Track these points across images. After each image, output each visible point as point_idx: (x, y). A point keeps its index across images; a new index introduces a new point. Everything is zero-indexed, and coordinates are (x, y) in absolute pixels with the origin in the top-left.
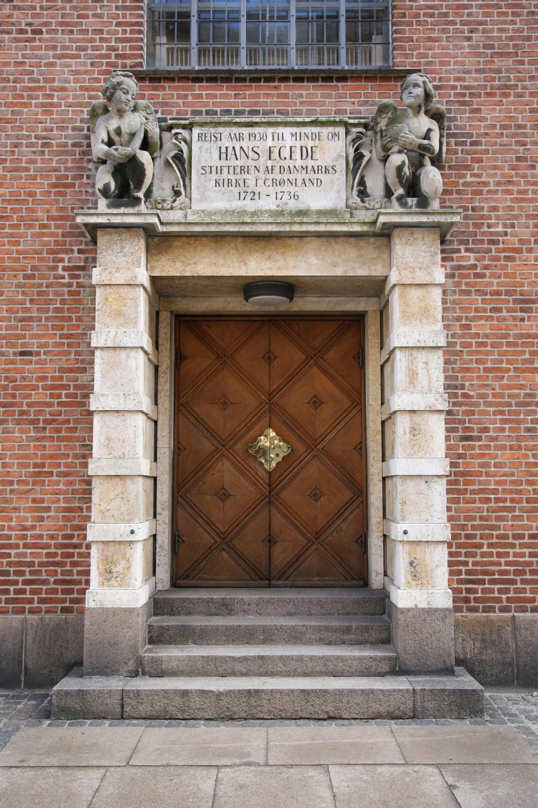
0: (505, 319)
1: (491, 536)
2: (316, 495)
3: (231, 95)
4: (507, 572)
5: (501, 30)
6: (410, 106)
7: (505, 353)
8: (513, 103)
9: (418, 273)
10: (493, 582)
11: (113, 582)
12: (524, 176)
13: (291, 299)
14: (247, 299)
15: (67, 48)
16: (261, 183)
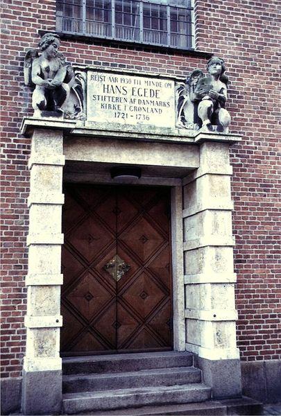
0: (256, 195)
1: (251, 317)
2: (144, 294)
3: (108, 54)
4: (260, 337)
5: (252, 38)
6: (213, 74)
7: (257, 214)
8: (258, 78)
9: (219, 167)
10: (253, 343)
11: (44, 354)
12: (264, 117)
13: (140, 177)
14: (113, 177)
15: (7, 11)
16: (128, 108)
